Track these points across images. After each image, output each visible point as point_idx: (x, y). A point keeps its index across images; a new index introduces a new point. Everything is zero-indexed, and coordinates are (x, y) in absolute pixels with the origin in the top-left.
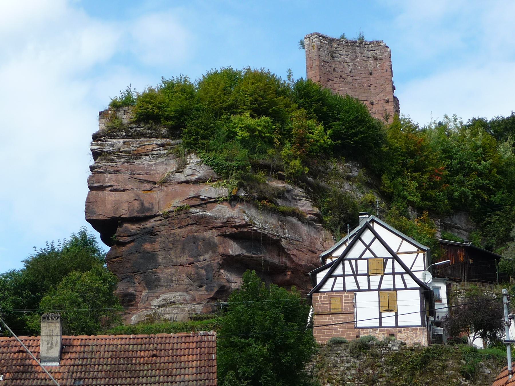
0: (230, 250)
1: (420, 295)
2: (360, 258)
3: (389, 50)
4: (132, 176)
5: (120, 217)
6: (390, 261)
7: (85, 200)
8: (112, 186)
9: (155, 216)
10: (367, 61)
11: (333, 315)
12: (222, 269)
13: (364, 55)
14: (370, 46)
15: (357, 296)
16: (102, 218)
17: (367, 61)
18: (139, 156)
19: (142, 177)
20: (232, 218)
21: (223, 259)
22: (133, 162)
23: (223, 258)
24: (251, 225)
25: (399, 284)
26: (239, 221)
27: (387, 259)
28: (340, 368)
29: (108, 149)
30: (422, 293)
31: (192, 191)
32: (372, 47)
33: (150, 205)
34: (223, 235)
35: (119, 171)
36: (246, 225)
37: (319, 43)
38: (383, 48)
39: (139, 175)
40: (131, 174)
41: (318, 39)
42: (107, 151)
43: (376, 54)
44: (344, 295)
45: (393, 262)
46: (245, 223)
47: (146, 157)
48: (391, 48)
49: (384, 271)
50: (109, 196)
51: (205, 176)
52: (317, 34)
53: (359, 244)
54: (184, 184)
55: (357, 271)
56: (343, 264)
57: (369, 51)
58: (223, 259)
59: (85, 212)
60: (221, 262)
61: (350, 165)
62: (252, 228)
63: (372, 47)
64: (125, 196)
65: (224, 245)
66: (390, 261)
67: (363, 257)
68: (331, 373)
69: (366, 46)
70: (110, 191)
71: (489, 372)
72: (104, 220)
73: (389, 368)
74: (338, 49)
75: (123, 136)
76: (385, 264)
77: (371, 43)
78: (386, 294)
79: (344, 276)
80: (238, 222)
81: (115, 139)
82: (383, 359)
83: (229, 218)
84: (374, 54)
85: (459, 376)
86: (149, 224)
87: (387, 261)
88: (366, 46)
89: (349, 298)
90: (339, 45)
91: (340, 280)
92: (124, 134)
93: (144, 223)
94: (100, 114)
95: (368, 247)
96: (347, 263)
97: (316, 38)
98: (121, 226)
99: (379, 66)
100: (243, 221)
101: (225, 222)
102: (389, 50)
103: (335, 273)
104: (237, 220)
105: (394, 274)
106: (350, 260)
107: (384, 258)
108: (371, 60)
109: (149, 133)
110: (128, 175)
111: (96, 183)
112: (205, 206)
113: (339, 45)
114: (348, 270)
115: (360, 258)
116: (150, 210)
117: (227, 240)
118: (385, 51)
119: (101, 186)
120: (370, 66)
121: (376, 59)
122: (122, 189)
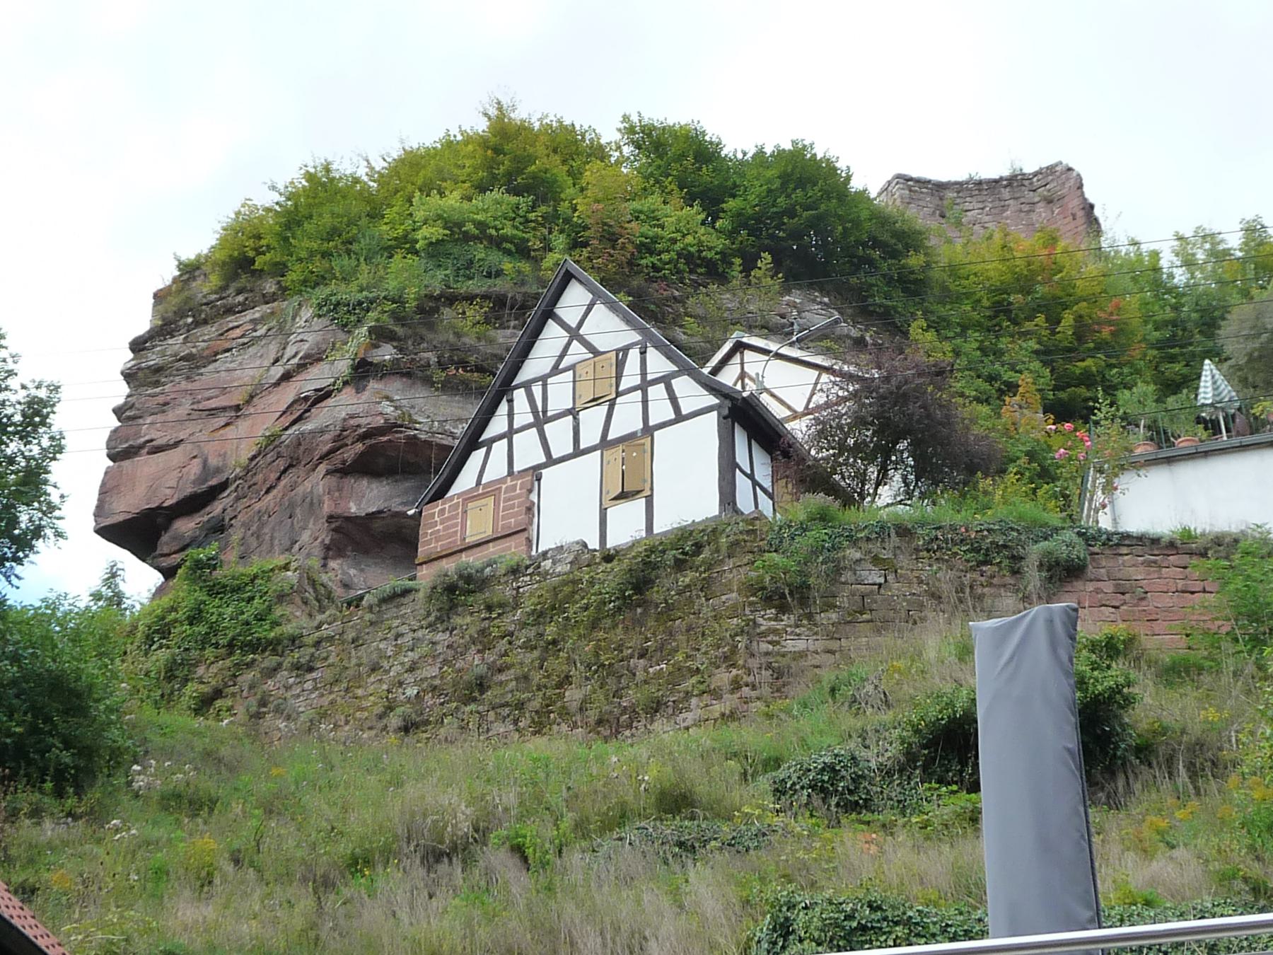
0: (352, 504)
1: (719, 425)
2: (556, 370)
3: (1075, 174)
4: (195, 407)
5: (159, 508)
6: (634, 354)
7: (98, 488)
8: (152, 441)
9: (224, 486)
10: (1030, 211)
11: (469, 552)
12: (334, 558)
13: (1022, 200)
14: (1035, 179)
15: (542, 481)
16: (121, 518)
17: (1030, 211)
18: (213, 357)
19: (213, 404)
20: (352, 417)
21: (333, 530)
22: (199, 375)
23: (333, 526)
24: (401, 426)
25: (661, 410)
26: (369, 420)
27: (625, 350)
28: (387, 672)
29: (152, 363)
30: (725, 418)
31: (289, 393)
32: (1038, 180)
33: (220, 459)
34: (336, 471)
35: (168, 404)
36: (390, 427)
37: (907, 192)
38: (1062, 174)
39: (209, 399)
40: (193, 404)
41: (901, 186)
42: (149, 367)
43: (1049, 191)
44: (504, 486)
45: (643, 353)
46: (382, 421)
47: (227, 354)
48: (1077, 168)
49: (618, 386)
50: (146, 466)
51: (317, 344)
52: (899, 176)
53: (552, 328)
54: (284, 384)
55: (545, 412)
56: (510, 401)
57: (1034, 191)
58: (333, 530)
59: (95, 515)
60: (327, 542)
61: (798, 301)
62: (401, 432)
63: (1038, 180)
64: (175, 456)
65: (337, 494)
66: (634, 354)
67: (749, 472)
68: (360, 692)
69: (1026, 183)
70: (149, 453)
71: (882, 580)
72: (126, 522)
73: (532, 634)
74: (958, 201)
75: (189, 325)
76: (620, 365)
77: (1035, 174)
78: (616, 453)
79: (509, 434)
80: (365, 422)
81: (173, 337)
82: (519, 611)
83: (345, 420)
84: (1045, 193)
85: (751, 604)
86: (217, 508)
87: (625, 355)
88: (1026, 183)
89: (518, 491)
90: (958, 192)
91: (500, 448)
92: (190, 320)
93: (208, 509)
94: (156, 296)
95: (574, 334)
96: (519, 395)
97: (897, 183)
98: (166, 528)
99: (1058, 214)
100: (379, 418)
101: (339, 435)
102: (1075, 174)
103: (487, 435)
104: (363, 421)
105: (644, 386)
106: (527, 385)
107: (618, 351)
108: (1041, 208)
109: (239, 304)
110: (187, 406)
111: (120, 444)
112: (307, 414)
113: (958, 192)
114: (523, 415)
115: (556, 370)
116: (218, 470)
117: (350, 481)
118: (1068, 179)
119: (131, 447)
120: (1037, 220)
121: (1050, 201)
122: (172, 442)
